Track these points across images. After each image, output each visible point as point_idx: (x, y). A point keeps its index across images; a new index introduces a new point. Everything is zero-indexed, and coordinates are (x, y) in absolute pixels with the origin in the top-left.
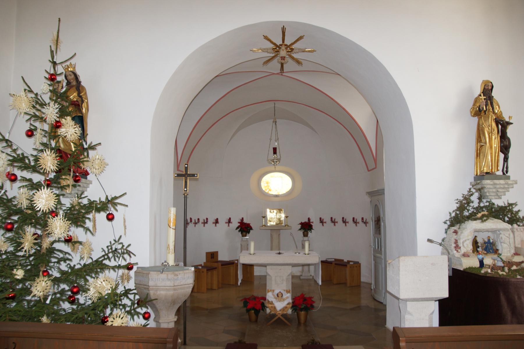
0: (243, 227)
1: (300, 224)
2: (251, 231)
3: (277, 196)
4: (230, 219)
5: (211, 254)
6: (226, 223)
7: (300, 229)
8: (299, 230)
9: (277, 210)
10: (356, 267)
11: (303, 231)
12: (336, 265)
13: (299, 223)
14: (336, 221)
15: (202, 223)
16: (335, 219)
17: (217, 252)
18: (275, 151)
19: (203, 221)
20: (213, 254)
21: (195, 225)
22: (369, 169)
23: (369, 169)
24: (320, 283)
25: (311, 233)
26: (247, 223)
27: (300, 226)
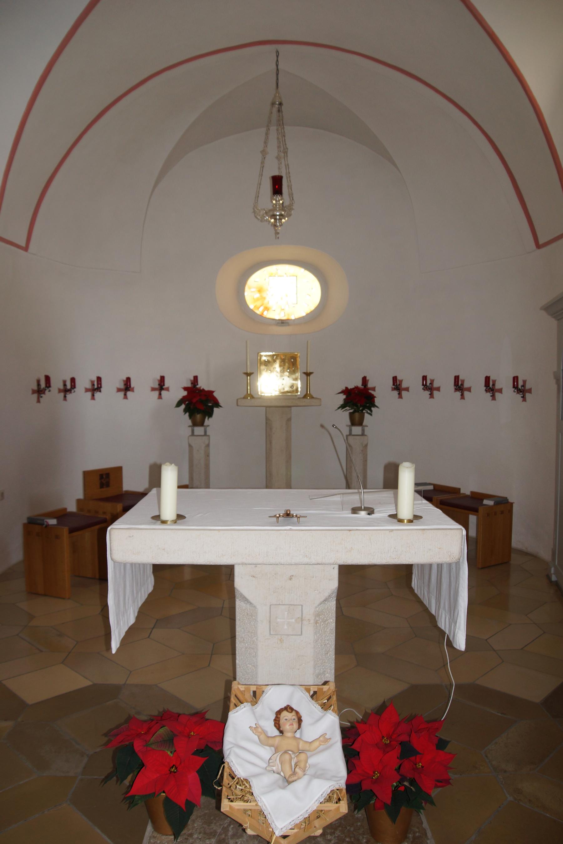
0: (195, 400)
2: (215, 409)
3: (283, 323)
5: (101, 476)
6: (153, 389)
7: (343, 407)
8: (339, 408)
10: (502, 512)
11: (351, 411)
13: (340, 391)
14: (435, 385)
17: (119, 470)
19: (89, 386)
20: (108, 475)
23: (541, 242)
24: (461, 643)
26: (206, 389)
27: (343, 397)
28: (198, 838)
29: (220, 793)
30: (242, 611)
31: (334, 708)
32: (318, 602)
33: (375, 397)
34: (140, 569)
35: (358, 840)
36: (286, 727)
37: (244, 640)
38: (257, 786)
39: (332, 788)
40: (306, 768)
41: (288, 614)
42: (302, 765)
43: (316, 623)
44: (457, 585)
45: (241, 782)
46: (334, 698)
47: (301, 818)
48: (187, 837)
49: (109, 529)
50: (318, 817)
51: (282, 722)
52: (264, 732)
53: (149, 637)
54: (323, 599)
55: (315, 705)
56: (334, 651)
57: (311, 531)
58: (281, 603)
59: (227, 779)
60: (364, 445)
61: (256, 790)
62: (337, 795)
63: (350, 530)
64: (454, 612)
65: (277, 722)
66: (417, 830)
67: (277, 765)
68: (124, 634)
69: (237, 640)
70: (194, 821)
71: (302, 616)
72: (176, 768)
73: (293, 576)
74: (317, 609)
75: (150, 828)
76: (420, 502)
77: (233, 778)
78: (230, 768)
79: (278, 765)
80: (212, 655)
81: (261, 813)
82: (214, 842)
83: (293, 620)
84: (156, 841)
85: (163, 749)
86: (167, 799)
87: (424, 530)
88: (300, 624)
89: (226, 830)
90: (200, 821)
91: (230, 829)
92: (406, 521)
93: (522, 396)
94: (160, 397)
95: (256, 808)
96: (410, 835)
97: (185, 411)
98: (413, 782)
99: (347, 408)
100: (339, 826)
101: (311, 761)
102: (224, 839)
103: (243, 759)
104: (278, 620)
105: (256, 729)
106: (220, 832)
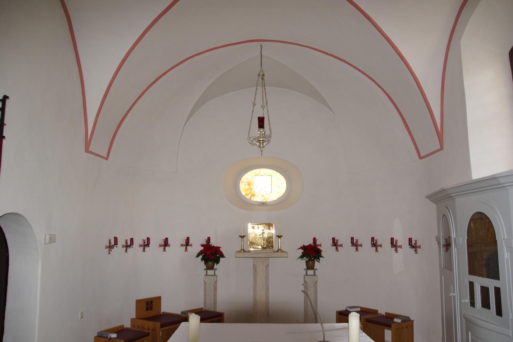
0: (208, 253)
1: (301, 248)
2: (221, 259)
4: (167, 239)
5: (147, 303)
8: (299, 258)
9: (264, 225)
10: (407, 327)
12: (368, 323)
15: (123, 246)
16: (357, 241)
18: (261, 122)
20: (151, 302)
21: (126, 250)
22: (422, 155)
25: (318, 263)
27: (301, 251)
60: (315, 282)
93: (415, 250)
94: (186, 250)
97: (202, 259)
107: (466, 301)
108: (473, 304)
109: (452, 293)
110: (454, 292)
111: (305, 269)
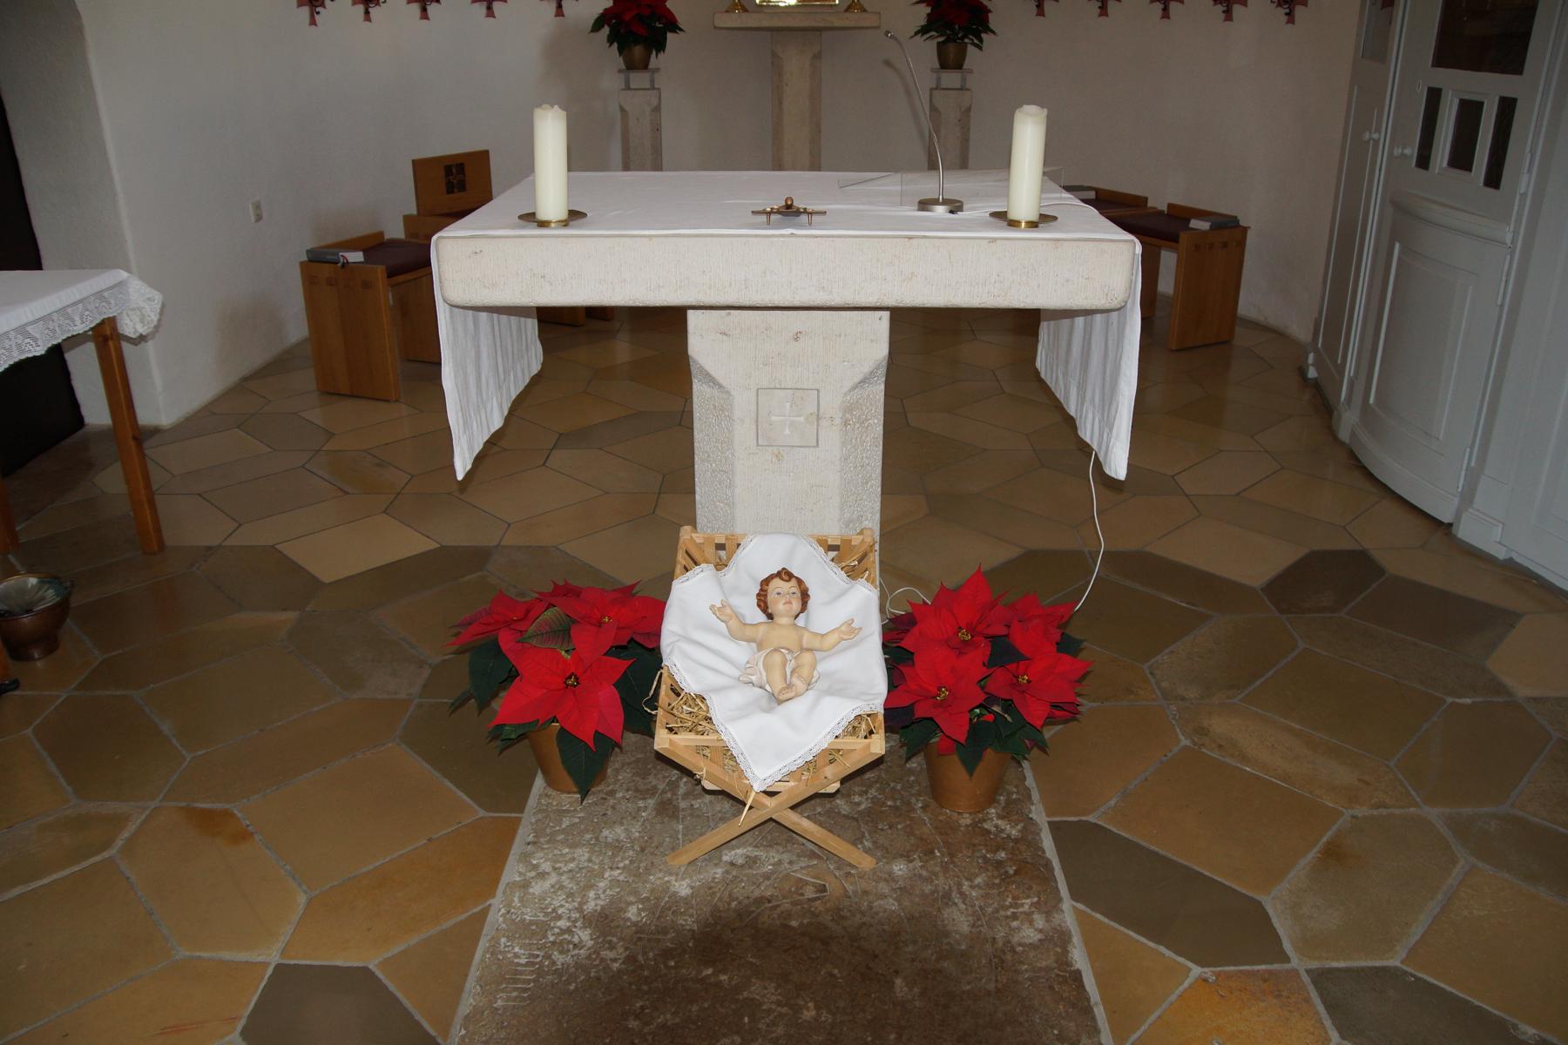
0: (627, 17)
2: (670, 36)
5: (448, 170)
7: (923, 31)
8: (916, 34)
10: (1225, 245)
17: (482, 157)
20: (461, 167)
21: (367, 13)
24: (1118, 466)
28: (624, 797)
29: (651, 719)
30: (704, 402)
31: (869, 575)
32: (848, 384)
33: (990, 11)
34: (510, 327)
35: (909, 803)
36: (778, 606)
37: (708, 456)
38: (719, 708)
39: (857, 712)
40: (812, 677)
41: (791, 406)
42: (805, 672)
43: (846, 423)
44: (1119, 355)
45: (691, 702)
46: (875, 558)
47: (800, 762)
48: (604, 796)
49: (434, 238)
50: (831, 762)
51: (771, 597)
52: (737, 616)
53: (544, 464)
54: (857, 379)
55: (835, 570)
56: (880, 478)
57: (831, 239)
58: (778, 386)
59: (667, 695)
60: (963, 109)
61: (717, 714)
62: (868, 724)
63: (910, 238)
64: (1109, 408)
65: (763, 598)
66: (1015, 790)
67: (758, 673)
68: (481, 446)
69: (696, 456)
70: (617, 771)
71: (818, 410)
72: (577, 679)
73: (800, 333)
74: (848, 398)
75: (539, 782)
76: (1058, 195)
77: (678, 695)
78: (671, 676)
79: (760, 672)
80: (659, 493)
81: (726, 751)
82: (651, 805)
83: (802, 419)
84: (550, 801)
85: (552, 646)
86: (563, 732)
87: (1058, 240)
88: (815, 426)
89: (673, 786)
90: (628, 771)
91: (682, 784)
92: (1023, 224)
93: (1287, 11)
95: (720, 744)
96: (1002, 798)
97: (611, 40)
98: (1008, 706)
99: (933, 33)
100: (877, 782)
101: (821, 667)
102: (670, 800)
103: (693, 660)
104: (773, 418)
105: (723, 612)
106: (665, 788)
107: (1407, 151)
108: (1424, 161)
109: (1373, 131)
110: (1378, 130)
111: (933, 70)
